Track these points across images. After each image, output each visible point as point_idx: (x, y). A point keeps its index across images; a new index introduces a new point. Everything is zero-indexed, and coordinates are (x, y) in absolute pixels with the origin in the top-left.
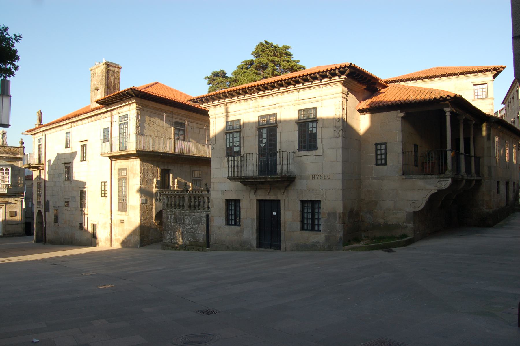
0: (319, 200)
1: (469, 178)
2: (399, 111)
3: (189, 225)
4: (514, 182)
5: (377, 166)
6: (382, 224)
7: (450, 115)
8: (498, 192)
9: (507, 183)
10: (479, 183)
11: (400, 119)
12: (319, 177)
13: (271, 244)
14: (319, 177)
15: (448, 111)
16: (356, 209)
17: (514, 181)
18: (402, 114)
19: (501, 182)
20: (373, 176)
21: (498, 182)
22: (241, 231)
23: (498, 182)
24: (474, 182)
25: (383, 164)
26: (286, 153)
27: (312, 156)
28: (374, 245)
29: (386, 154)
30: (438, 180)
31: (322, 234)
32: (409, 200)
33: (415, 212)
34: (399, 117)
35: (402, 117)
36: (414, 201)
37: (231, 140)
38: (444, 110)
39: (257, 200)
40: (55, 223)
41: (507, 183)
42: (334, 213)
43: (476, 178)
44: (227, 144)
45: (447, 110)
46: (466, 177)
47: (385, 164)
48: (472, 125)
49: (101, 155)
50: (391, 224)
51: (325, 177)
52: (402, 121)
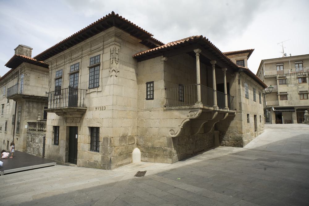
0: (98, 126)
1: (221, 110)
2: (162, 56)
3: (37, 143)
4: (260, 116)
5: (148, 100)
6: (150, 147)
7: (199, 55)
8: (248, 121)
9: (255, 116)
10: (232, 116)
11: (163, 62)
12: (99, 109)
13: (74, 158)
14: (99, 109)
15: (197, 52)
16: (130, 134)
17: (260, 115)
18: (164, 59)
19: (250, 115)
20: (145, 108)
21: (248, 115)
22: (58, 150)
23: (248, 115)
24: (228, 114)
25: (152, 98)
26: (82, 91)
27: (96, 92)
28: (193, 164)
29: (153, 91)
30: (190, 110)
31: (100, 155)
32: (169, 128)
33: (173, 138)
34: (162, 61)
35: (165, 61)
36: (173, 128)
37: (73, 79)
38: (194, 51)
39: (67, 126)
40: (272, 123)
41: (255, 116)
42: (107, 138)
43: (229, 110)
44: (95, 80)
45: (197, 51)
46: (218, 109)
47: (153, 99)
48: (214, 65)
49: (290, 54)
50: (156, 147)
51: (102, 108)
52: (164, 64)
